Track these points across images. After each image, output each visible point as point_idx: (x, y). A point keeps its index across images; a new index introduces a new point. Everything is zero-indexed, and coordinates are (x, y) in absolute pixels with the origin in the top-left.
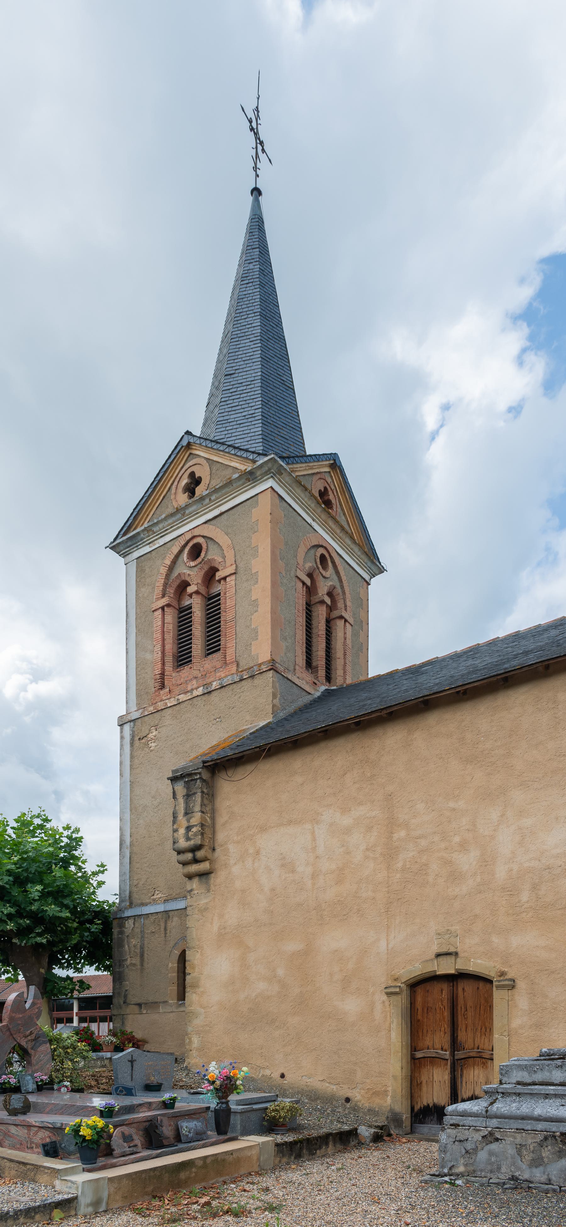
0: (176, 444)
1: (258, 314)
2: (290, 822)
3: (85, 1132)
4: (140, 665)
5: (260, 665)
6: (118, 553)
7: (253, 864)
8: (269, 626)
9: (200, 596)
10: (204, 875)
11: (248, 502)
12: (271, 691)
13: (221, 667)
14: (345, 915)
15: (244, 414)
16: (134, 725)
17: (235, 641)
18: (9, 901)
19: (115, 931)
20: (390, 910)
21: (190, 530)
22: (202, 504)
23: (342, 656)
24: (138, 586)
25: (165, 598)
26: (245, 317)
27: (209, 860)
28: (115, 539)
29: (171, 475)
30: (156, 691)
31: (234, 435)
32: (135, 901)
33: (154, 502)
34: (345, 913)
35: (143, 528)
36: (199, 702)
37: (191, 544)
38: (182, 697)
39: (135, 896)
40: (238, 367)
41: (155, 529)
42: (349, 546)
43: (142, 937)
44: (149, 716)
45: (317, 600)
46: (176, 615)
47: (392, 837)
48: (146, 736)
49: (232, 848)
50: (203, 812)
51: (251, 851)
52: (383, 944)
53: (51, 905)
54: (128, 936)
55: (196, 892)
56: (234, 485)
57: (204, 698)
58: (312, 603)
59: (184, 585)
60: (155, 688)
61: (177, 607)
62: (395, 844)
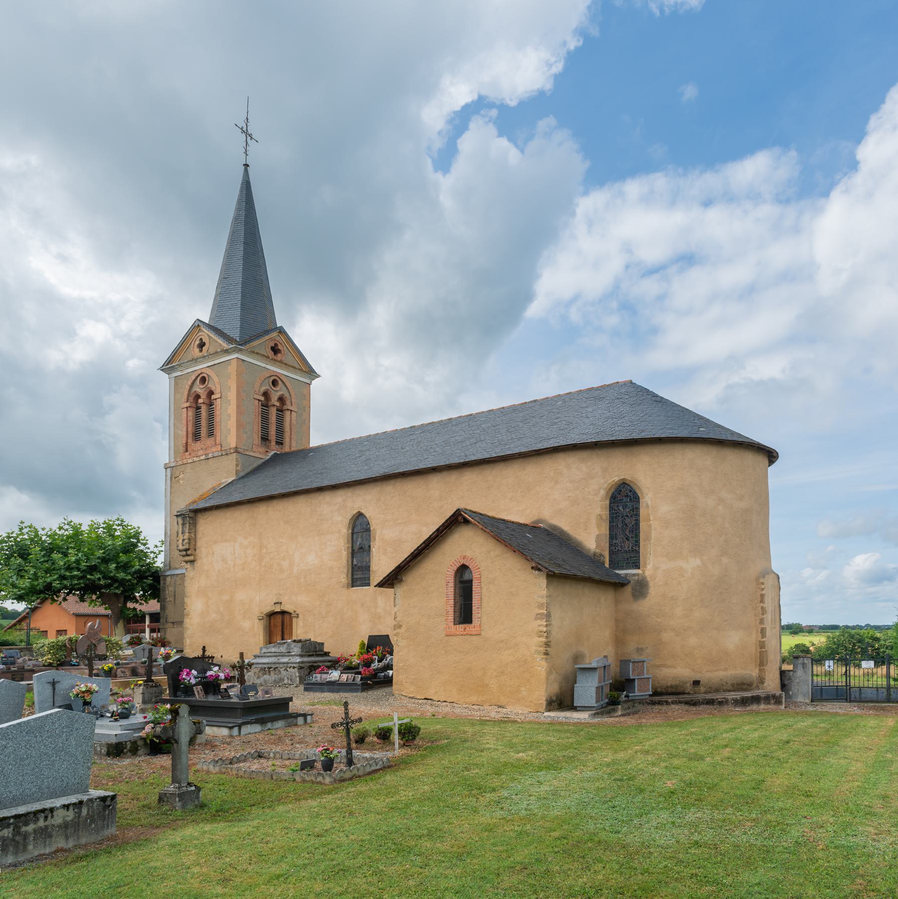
2: (226, 541)
3: (106, 668)
4: (176, 437)
5: (230, 449)
10: (192, 562)
12: (235, 463)
18: (99, 572)
19: (162, 582)
23: (289, 431)
32: (172, 567)
38: (195, 459)
39: (172, 563)
43: (175, 586)
49: (203, 550)
50: (189, 533)
51: (211, 552)
52: (258, 598)
59: (198, 397)
61: (195, 406)
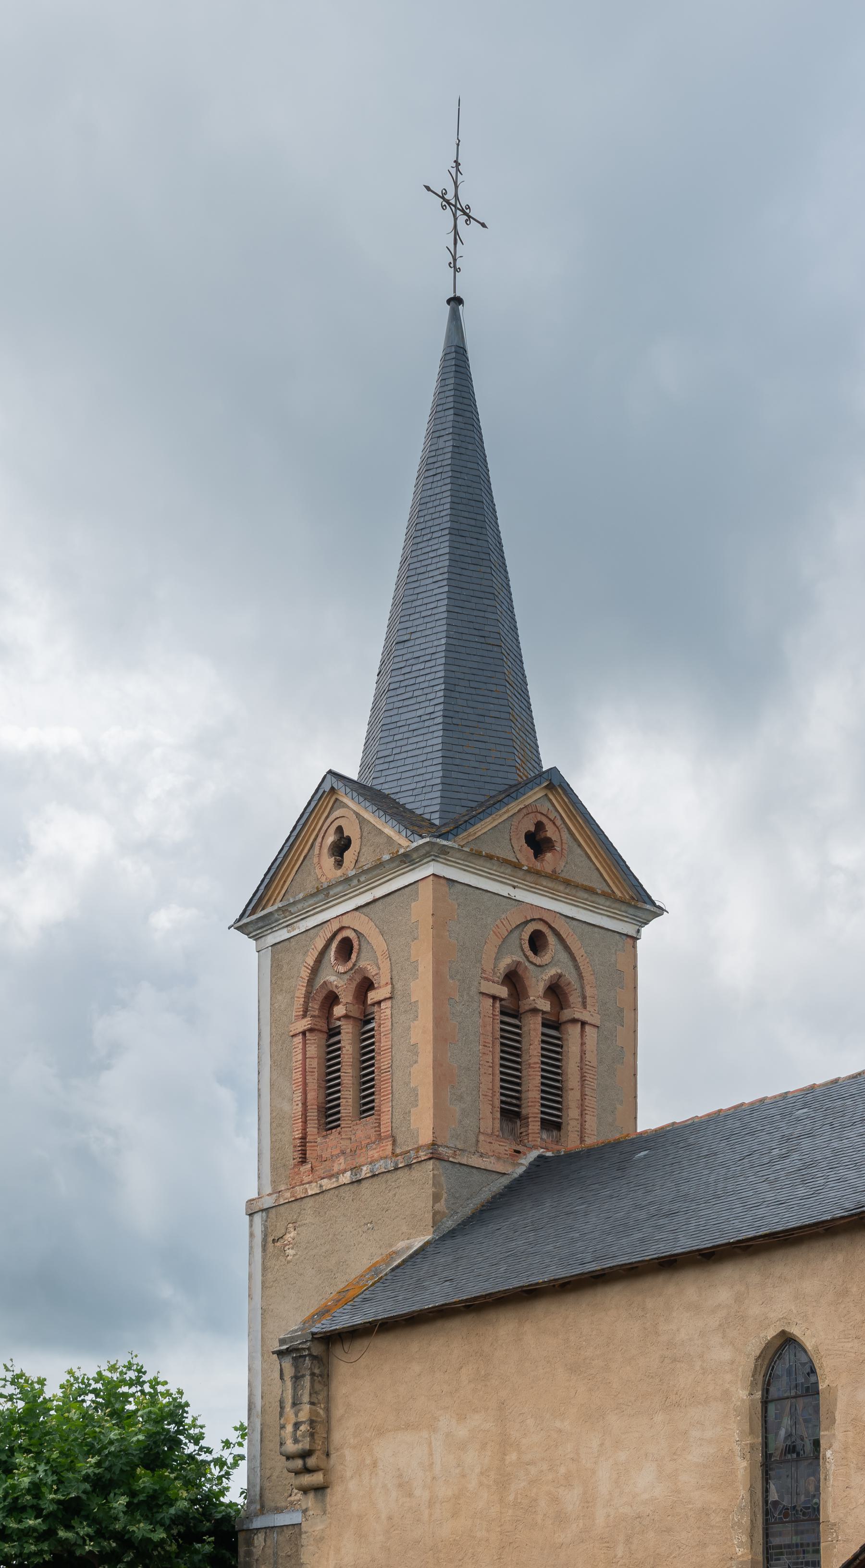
0: (316, 786)
1: (447, 532)
2: (408, 1427)
4: (277, 1120)
6: (248, 935)
7: (371, 1479)
8: (431, 1089)
9: (351, 1021)
10: (320, 1490)
11: (406, 889)
13: (374, 1143)
14: (460, 1560)
15: (419, 713)
16: (267, 1217)
17: (391, 1104)
18: (86, 1518)
20: (503, 1557)
21: (337, 916)
22: (350, 885)
24: (273, 990)
25: (306, 1020)
26: (429, 536)
27: (322, 1469)
28: (242, 916)
29: (312, 828)
30: (295, 1165)
31: (404, 749)
32: (269, 1504)
33: (293, 863)
34: (460, 1557)
35: (275, 907)
36: (346, 1193)
37: (339, 937)
38: (327, 1184)
39: (268, 1495)
40: (414, 629)
41: (293, 910)
42: (586, 900)
44: (286, 1206)
45: (527, 1008)
46: (324, 1042)
47: (505, 1460)
48: (282, 1237)
53: (139, 1522)
54: (257, 1560)
55: (311, 1513)
56: (387, 866)
57: (353, 1188)
58: (521, 1011)
60: (294, 1159)
61: (325, 1029)
62: (507, 1469)
